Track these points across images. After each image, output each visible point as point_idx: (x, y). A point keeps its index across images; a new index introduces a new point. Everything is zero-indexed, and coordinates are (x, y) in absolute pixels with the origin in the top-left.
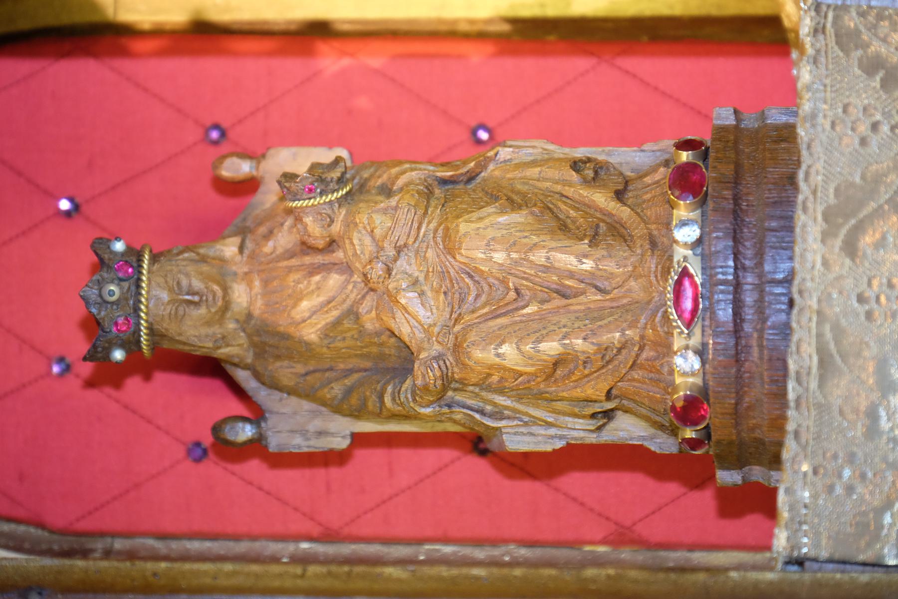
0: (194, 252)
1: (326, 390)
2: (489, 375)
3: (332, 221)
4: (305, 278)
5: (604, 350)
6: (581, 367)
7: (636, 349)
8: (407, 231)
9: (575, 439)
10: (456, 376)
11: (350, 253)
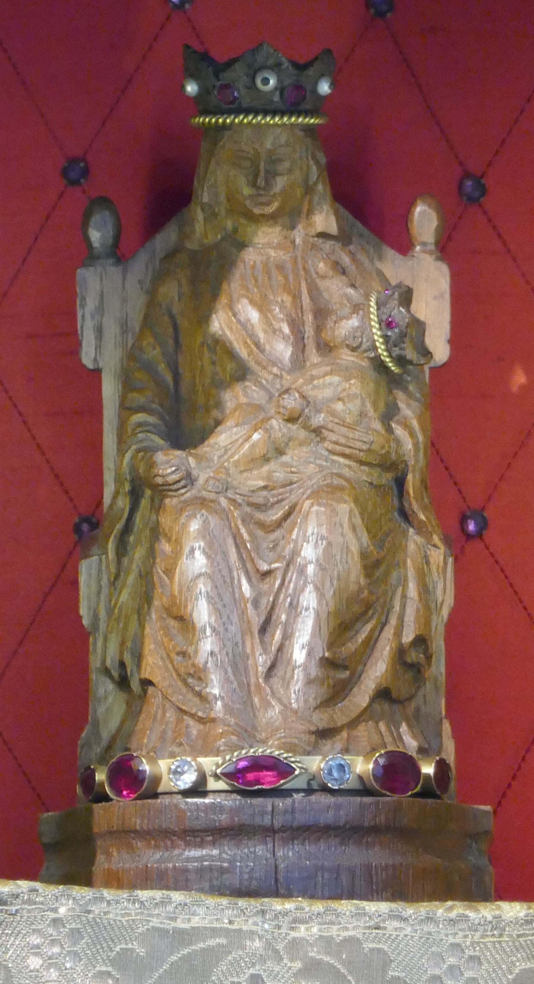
1: (151, 340)
2: (169, 540)
3: (354, 349)
4: (287, 315)
5: (199, 675)
7: (200, 714)
9: (95, 643)
10: (167, 501)
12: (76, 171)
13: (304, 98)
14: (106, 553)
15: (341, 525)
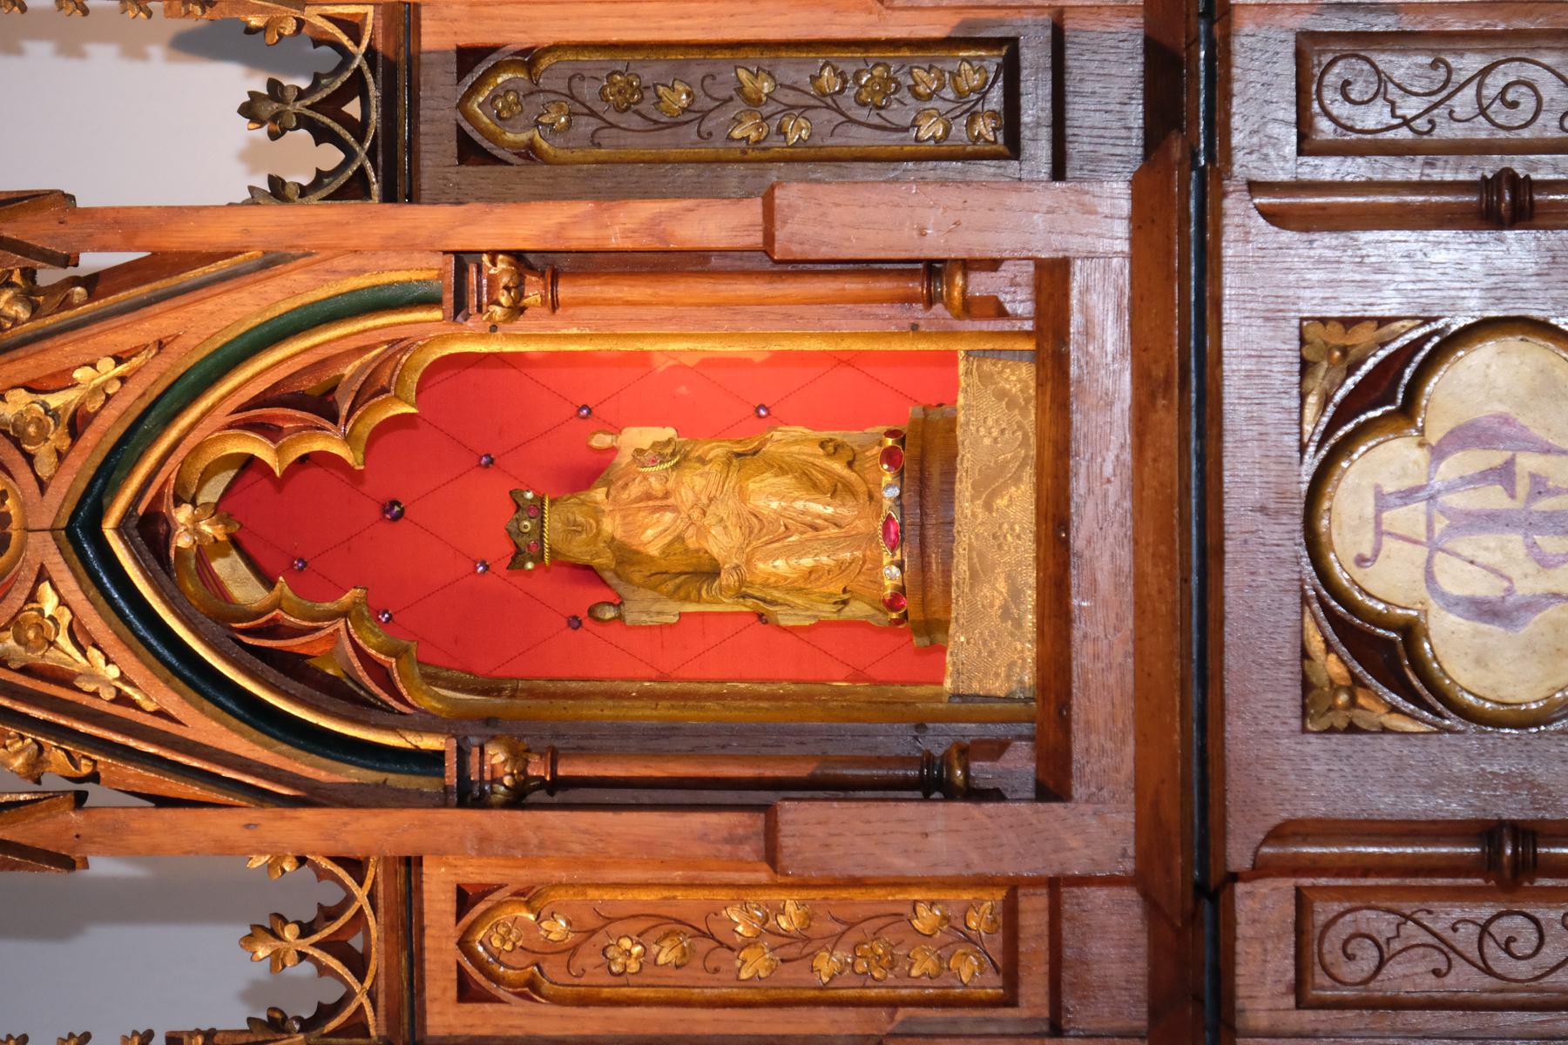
12: (575, 623)
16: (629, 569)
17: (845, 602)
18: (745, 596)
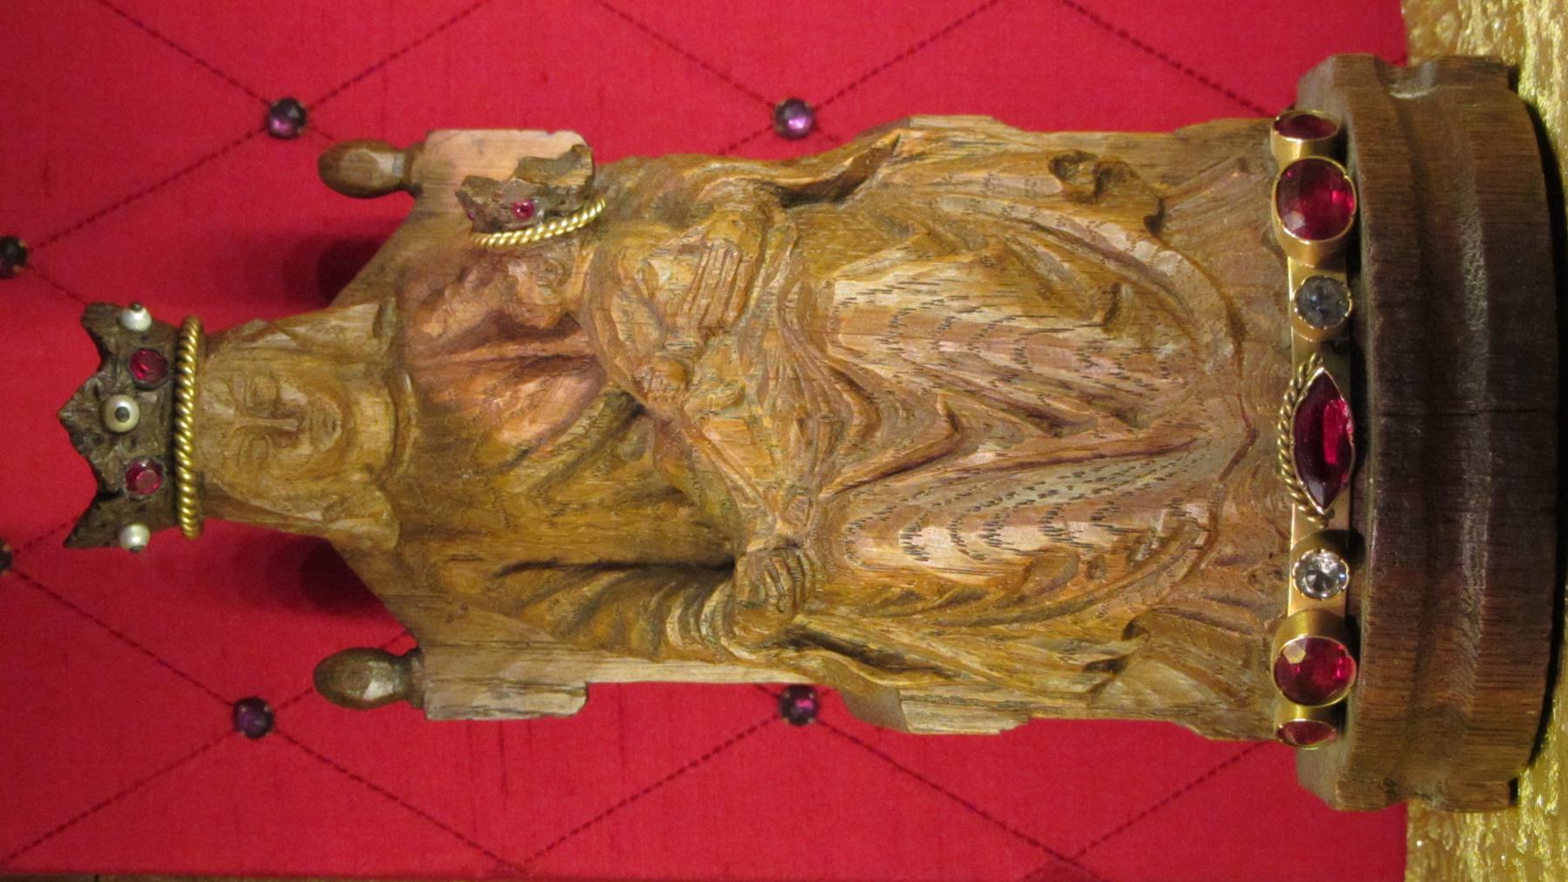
0: (286, 332)
1: (544, 606)
3: (567, 274)
6: (1082, 578)
8: (725, 296)
9: (1045, 709)
11: (603, 338)
12: (253, 717)
13: (152, 351)
14: (897, 689)
15: (873, 292)
16: (437, 552)
17: (1115, 666)
18: (803, 640)
